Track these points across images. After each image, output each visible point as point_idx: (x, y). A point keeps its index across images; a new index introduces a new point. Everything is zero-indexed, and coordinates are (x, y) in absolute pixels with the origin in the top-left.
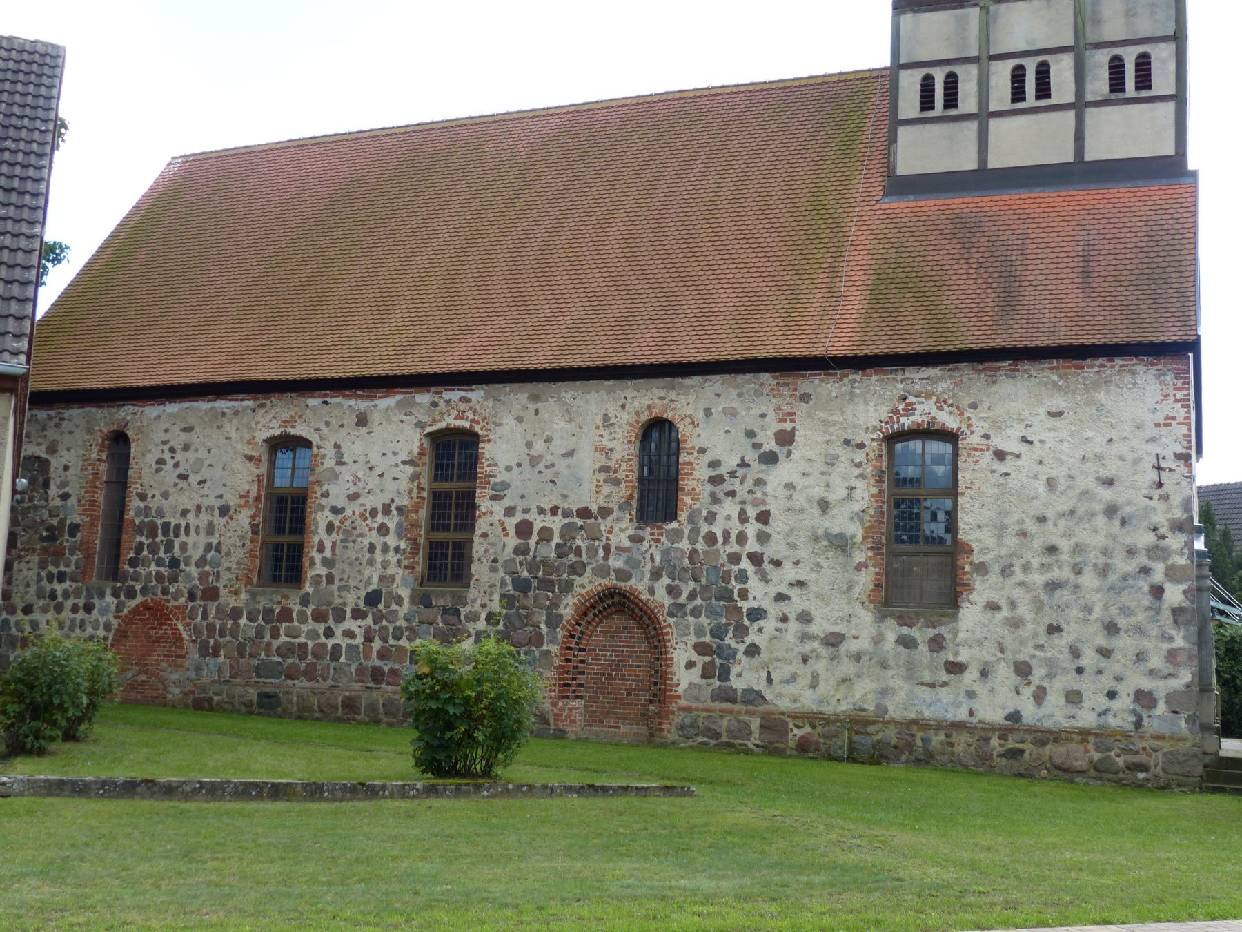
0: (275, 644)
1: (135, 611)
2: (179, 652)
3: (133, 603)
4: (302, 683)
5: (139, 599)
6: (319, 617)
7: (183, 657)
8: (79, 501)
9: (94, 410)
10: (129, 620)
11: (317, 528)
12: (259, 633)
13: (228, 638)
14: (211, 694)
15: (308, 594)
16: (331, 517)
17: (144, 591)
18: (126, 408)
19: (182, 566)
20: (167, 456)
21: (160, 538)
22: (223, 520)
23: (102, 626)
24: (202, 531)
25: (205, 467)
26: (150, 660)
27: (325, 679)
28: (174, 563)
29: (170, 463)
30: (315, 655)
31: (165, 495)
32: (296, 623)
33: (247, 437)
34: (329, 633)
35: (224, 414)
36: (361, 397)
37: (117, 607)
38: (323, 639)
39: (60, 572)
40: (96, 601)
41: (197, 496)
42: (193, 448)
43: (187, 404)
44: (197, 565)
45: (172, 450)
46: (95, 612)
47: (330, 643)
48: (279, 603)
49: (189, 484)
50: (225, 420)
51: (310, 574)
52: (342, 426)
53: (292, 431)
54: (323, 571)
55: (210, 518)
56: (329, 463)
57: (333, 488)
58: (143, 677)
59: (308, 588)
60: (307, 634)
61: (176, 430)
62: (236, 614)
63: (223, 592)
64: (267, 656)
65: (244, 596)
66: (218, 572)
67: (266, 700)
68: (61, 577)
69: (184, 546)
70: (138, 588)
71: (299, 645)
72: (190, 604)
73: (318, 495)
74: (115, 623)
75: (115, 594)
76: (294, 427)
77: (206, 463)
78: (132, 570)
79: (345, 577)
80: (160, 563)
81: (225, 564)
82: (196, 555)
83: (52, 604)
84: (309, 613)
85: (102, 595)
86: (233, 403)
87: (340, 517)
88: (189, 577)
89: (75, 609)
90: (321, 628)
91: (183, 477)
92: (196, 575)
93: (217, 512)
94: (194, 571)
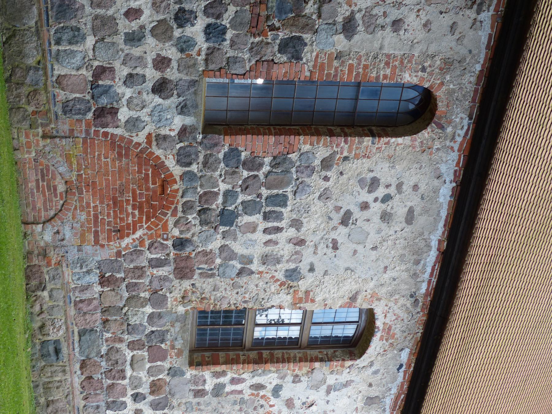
0: (123, 346)
1: (159, 166)
2: (102, 237)
3: (171, 163)
4: (77, 380)
5: (177, 171)
6: (155, 387)
7: (97, 242)
8: (339, 56)
9: (478, 67)
10: (144, 158)
11: (260, 375)
12: (131, 329)
13: (126, 295)
14: (49, 287)
15: (183, 374)
16: (270, 387)
17: (188, 177)
18: (466, 122)
19: (222, 229)
20: (381, 192)
21: (265, 192)
22: (280, 276)
23: (134, 114)
24: (268, 249)
25: (355, 246)
26: (87, 196)
27: (86, 398)
28: (227, 218)
29: (369, 198)
30: (111, 387)
31: (325, 196)
32: (148, 365)
33: (383, 291)
34: (136, 397)
35: (417, 262)
36: (397, 398)
37: (165, 137)
38: (130, 392)
39: (224, 31)
40: (173, 101)
41: (317, 239)
42: (384, 226)
43: (444, 213)
44: (223, 248)
45: (387, 198)
46: (157, 100)
47: (128, 400)
48: (173, 347)
49: (335, 228)
50: (409, 265)
51: (207, 374)
52: (370, 385)
53: (378, 335)
54: (209, 387)
55: (286, 258)
56: (331, 380)
57: (301, 387)
58: (61, 188)
59: (190, 373)
60: (136, 377)
61: (414, 201)
62: (157, 298)
63: (186, 284)
64: (107, 341)
65: (181, 309)
66: (212, 275)
67: (51, 349)
68: (214, 32)
69: (253, 228)
70: (194, 168)
71: (123, 371)
72: (170, 243)
73: (297, 372)
74: (141, 138)
75: (184, 131)
76: (381, 339)
77: (360, 248)
78: (221, 156)
79: (202, 407)
80: (229, 195)
81: (223, 283)
82: (238, 248)
83: (169, 16)
84: (161, 377)
85: (183, 109)
86: (429, 270)
87: (269, 395)
88: (208, 239)
89: (161, 63)
90: (144, 390)
91: (345, 220)
92: (210, 247)
93: (292, 266)
94: (215, 244)
